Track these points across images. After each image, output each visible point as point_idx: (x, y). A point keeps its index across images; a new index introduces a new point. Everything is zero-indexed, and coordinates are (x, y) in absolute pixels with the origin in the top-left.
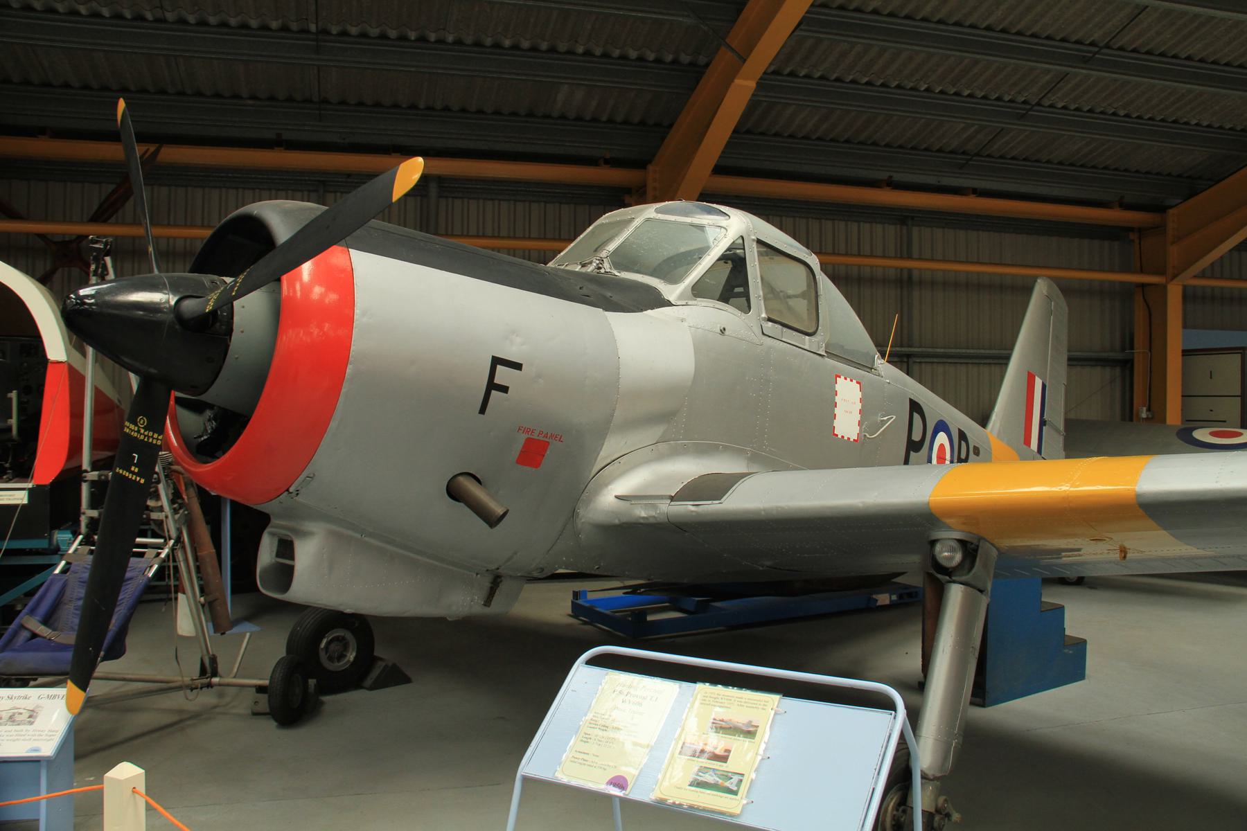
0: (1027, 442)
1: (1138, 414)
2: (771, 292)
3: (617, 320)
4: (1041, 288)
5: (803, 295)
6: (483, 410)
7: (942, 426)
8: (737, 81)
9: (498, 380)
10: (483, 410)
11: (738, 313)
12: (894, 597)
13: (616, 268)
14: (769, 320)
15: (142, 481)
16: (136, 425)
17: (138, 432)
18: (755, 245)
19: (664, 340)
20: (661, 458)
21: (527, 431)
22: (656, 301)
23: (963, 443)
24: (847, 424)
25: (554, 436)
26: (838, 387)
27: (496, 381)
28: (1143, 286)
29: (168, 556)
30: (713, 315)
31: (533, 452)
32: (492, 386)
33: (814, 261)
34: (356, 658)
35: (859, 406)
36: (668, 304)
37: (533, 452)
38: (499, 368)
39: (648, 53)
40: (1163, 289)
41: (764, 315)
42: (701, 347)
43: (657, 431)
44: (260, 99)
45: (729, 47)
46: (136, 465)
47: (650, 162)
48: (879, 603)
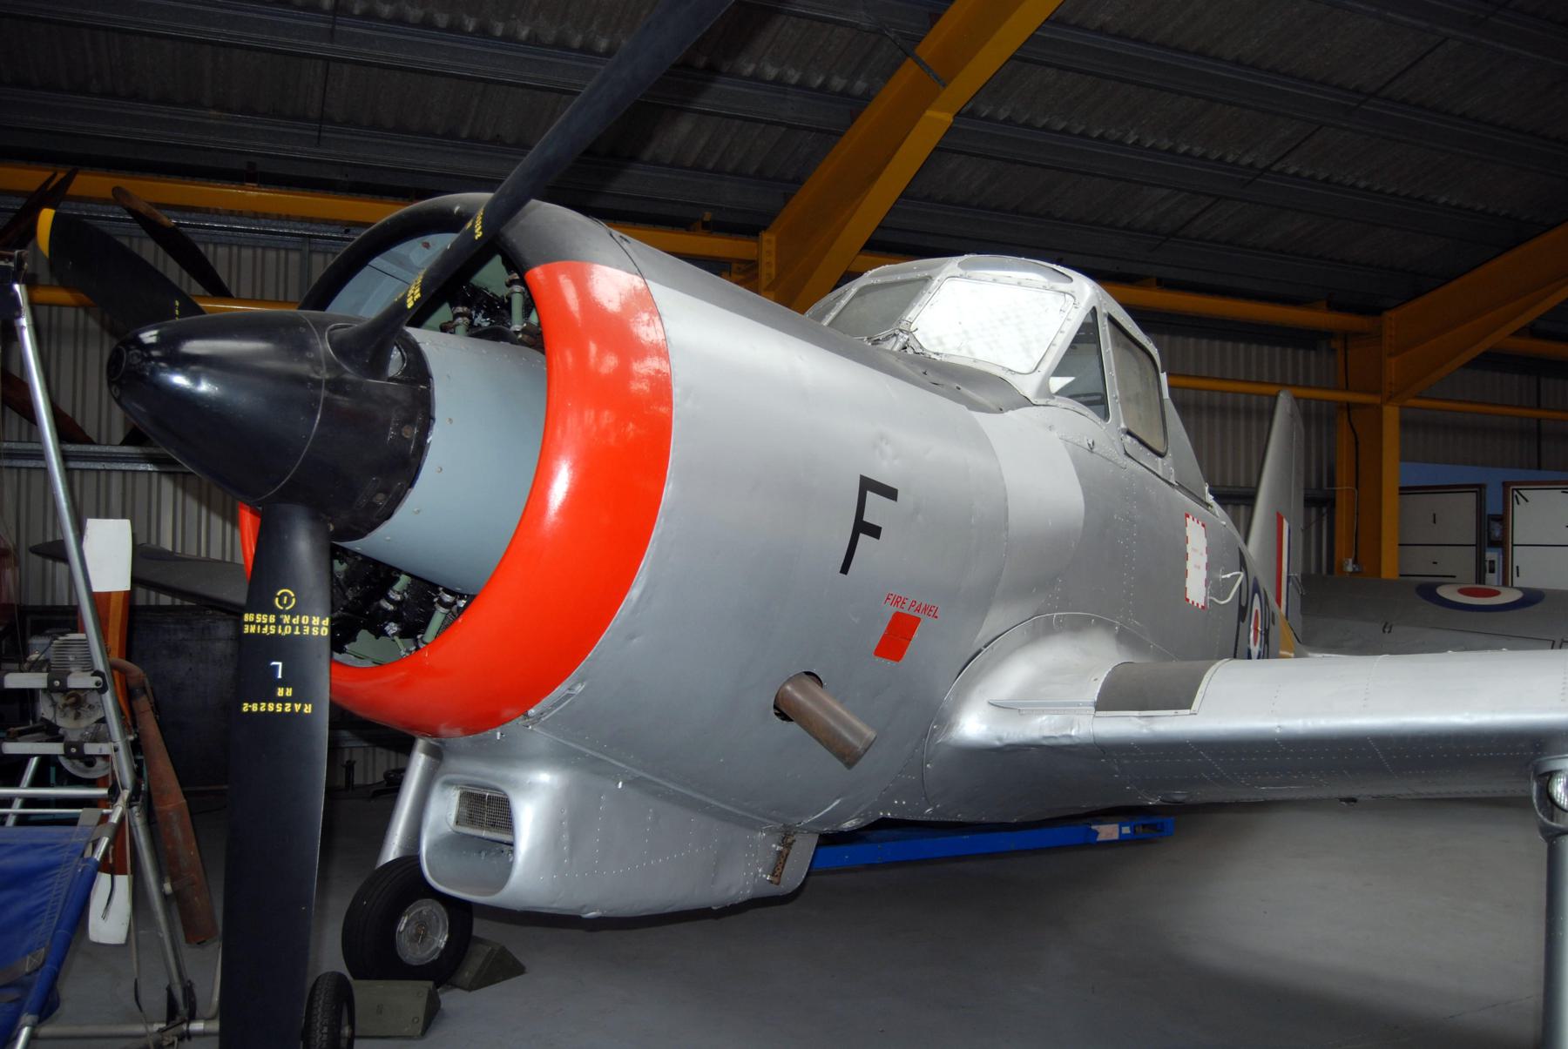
1: (1341, 567)
4: (1284, 403)
6: (845, 569)
8: (928, 113)
9: (868, 518)
10: (845, 569)
11: (1098, 419)
12: (1126, 830)
14: (1129, 433)
17: (279, 622)
21: (898, 601)
25: (928, 610)
28: (1349, 407)
29: (122, 818)
31: (898, 636)
32: (862, 527)
34: (448, 943)
37: (898, 636)
39: (791, 72)
40: (1378, 410)
41: (1123, 426)
44: (229, 110)
45: (917, 60)
46: (284, 683)
47: (765, 228)
48: (1101, 838)
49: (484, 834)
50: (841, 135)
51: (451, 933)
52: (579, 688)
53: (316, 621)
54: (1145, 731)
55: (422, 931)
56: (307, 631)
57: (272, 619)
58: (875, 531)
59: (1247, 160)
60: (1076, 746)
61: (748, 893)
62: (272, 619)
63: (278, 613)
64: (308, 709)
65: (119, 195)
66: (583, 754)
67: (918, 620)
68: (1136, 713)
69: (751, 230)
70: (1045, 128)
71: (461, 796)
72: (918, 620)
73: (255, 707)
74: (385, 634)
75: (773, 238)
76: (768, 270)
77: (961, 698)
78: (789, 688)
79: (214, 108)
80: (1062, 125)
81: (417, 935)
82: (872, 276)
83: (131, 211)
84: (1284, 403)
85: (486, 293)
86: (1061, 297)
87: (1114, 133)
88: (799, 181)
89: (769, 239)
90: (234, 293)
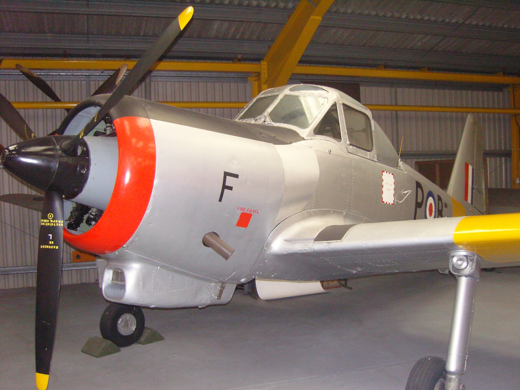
0: (466, 199)
2: (351, 132)
3: (280, 148)
4: (469, 119)
5: (364, 131)
6: (220, 200)
7: (430, 194)
8: (312, 17)
10: (220, 200)
13: (273, 121)
14: (351, 145)
15: (57, 247)
16: (47, 219)
17: (50, 222)
18: (342, 107)
19: (304, 157)
20: (304, 218)
22: (294, 137)
23: (440, 202)
24: (388, 196)
26: (383, 177)
27: (227, 184)
30: (325, 143)
31: (244, 220)
32: (225, 187)
33: (369, 113)
34: (136, 329)
35: (393, 186)
36: (304, 139)
37: (244, 220)
38: (228, 178)
42: (321, 162)
43: (303, 205)
46: (52, 240)
47: (262, 59)
49: (119, 283)
50: (285, 24)
51: (137, 326)
52: (137, 239)
53: (59, 221)
54: (327, 247)
55: (126, 325)
56: (57, 225)
57: (48, 221)
58: (230, 188)
59: (454, 21)
60: (309, 253)
61: (209, 302)
62: (48, 221)
63: (49, 220)
64: (57, 247)
65: (18, 67)
66: (144, 258)
67: (251, 215)
68: (325, 242)
69: (258, 59)
70: (368, 15)
71: (113, 272)
72: (251, 215)
73: (44, 247)
74: (91, 224)
75: (265, 63)
76: (264, 75)
77: (274, 238)
78: (207, 236)
79: (50, 33)
80: (374, 13)
81: (125, 326)
82: (262, 94)
83: (22, 72)
84: (469, 119)
85: (106, 122)
86: (323, 99)
87: (397, 15)
88: (273, 41)
89: (264, 64)
90: (62, 100)
